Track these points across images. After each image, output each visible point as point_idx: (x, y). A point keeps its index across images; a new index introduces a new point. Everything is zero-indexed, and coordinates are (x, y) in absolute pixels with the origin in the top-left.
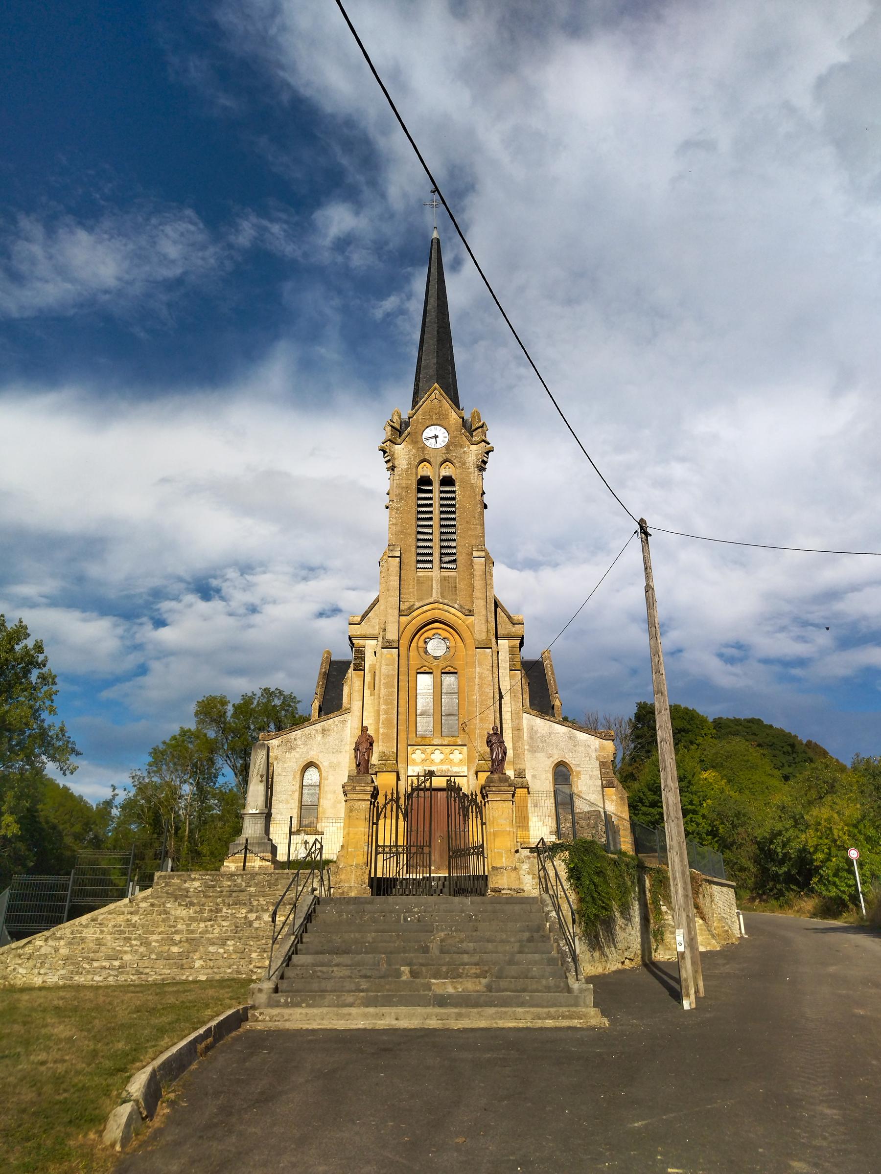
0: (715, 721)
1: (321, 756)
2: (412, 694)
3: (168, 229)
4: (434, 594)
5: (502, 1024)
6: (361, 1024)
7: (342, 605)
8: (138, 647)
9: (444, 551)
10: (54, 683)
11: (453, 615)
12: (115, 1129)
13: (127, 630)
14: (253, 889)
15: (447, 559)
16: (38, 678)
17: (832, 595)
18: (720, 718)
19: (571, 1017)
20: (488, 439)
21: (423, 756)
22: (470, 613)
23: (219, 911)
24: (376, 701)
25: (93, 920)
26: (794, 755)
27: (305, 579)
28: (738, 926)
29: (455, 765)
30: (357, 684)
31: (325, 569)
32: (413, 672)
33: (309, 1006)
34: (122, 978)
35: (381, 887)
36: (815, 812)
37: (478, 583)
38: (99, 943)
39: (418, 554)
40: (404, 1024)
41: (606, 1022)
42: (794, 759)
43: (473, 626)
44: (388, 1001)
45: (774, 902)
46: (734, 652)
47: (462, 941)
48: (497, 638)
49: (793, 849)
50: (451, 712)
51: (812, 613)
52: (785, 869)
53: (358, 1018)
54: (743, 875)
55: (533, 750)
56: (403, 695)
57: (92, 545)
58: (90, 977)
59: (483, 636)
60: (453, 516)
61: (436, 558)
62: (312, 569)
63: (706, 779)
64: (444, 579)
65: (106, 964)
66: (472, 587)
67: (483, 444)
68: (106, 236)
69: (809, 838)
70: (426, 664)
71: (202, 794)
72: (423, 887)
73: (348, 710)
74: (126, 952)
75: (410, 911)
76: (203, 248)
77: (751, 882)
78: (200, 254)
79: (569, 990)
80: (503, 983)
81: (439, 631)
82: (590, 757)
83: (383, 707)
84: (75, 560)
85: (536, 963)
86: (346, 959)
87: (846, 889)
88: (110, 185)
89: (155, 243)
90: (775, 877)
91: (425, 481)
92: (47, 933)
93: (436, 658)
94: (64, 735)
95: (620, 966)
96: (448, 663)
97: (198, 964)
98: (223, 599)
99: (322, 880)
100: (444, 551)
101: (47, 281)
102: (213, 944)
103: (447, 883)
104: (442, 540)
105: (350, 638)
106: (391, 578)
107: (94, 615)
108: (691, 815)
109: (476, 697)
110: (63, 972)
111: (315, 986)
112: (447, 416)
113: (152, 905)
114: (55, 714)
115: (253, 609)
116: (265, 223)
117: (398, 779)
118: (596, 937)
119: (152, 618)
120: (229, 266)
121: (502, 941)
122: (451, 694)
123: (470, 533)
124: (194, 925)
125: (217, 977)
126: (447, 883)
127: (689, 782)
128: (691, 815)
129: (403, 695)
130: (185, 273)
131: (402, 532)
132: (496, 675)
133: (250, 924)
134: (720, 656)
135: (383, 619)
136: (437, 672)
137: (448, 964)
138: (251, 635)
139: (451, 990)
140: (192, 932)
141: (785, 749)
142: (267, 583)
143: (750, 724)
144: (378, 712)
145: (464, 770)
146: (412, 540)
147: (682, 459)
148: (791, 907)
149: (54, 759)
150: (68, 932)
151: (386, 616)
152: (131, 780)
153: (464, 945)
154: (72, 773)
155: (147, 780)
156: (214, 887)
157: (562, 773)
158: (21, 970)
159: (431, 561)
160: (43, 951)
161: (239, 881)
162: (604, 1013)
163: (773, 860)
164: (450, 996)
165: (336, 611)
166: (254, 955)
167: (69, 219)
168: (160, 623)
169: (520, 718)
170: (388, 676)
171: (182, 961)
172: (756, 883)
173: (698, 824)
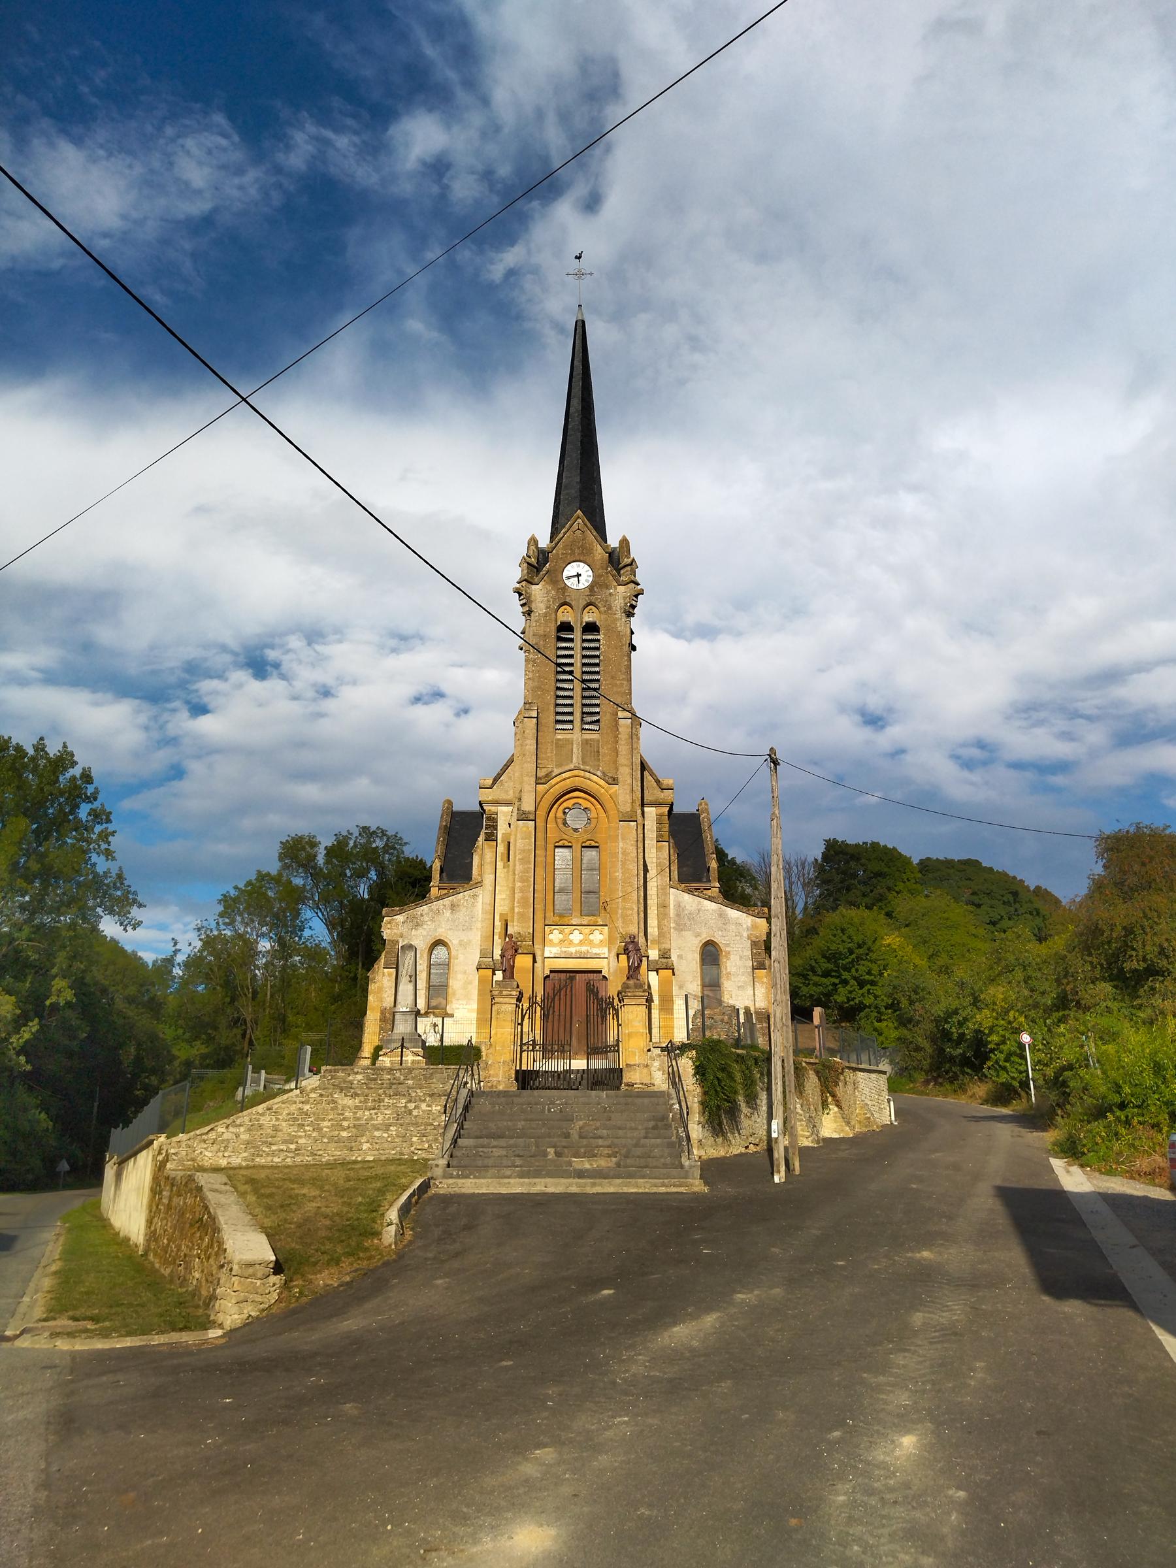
0: (922, 862)
1: (450, 933)
2: (550, 869)
3: (190, 143)
4: (575, 760)
5: (626, 1190)
6: (519, 1190)
7: (445, 688)
8: (172, 741)
9: (586, 710)
10: (109, 821)
11: (595, 782)
12: (389, 1234)
13: (155, 718)
14: (410, 1082)
15: (589, 719)
16: (89, 814)
17: (1112, 676)
18: (928, 859)
19: (680, 1186)
20: (638, 578)
21: (561, 936)
22: (614, 781)
23: (380, 1101)
24: (511, 878)
25: (268, 1109)
26: (1017, 906)
27: (394, 650)
28: (886, 1113)
29: (595, 946)
30: (489, 856)
31: (422, 638)
32: (550, 846)
33: (475, 1177)
34: (298, 1159)
35: (525, 1079)
36: (991, 990)
37: (623, 748)
38: (276, 1129)
39: (558, 713)
40: (551, 1190)
41: (706, 1189)
42: (1016, 910)
43: (617, 796)
44: (537, 1174)
45: (948, 1086)
46: (976, 753)
47: (597, 1129)
48: (643, 805)
49: (969, 1030)
50: (591, 889)
51: (1082, 701)
52: (960, 1051)
53: (516, 1186)
54: (919, 1056)
55: (680, 928)
56: (540, 872)
57: (99, 601)
58: (269, 1159)
59: (628, 808)
60: (597, 669)
61: (577, 717)
62: (403, 638)
63: (889, 945)
64: (586, 743)
65: (283, 1147)
66: (616, 752)
67: (632, 585)
68: (101, 153)
69: (983, 1019)
70: (565, 837)
71: (284, 949)
72: (563, 1080)
73: (479, 884)
74: (300, 1137)
75: (553, 1103)
76: (240, 171)
77: (926, 1064)
78: (236, 181)
79: (682, 1166)
80: (629, 1161)
81: (580, 801)
82: (742, 936)
83: (518, 884)
84: (72, 621)
85: (658, 1146)
86: (502, 1142)
87: (1016, 1075)
88: (103, 73)
89: (171, 164)
90: (952, 1059)
91: (566, 627)
92: (228, 1121)
93: (576, 830)
94: (122, 884)
95: (743, 1150)
96: (589, 837)
97: (365, 1146)
98: (283, 677)
99: (473, 1075)
100: (586, 710)
101: (20, 217)
102: (378, 1129)
103: (585, 1076)
104: (584, 697)
105: (480, 804)
106: (528, 742)
107: (109, 696)
108: (869, 986)
109: (619, 874)
110: (245, 1155)
111: (479, 1163)
112: (590, 551)
113: (321, 1095)
114: (114, 859)
115: (326, 692)
116: (328, 134)
117: (534, 961)
118: (720, 1124)
119: (188, 702)
120: (277, 199)
121: (631, 1128)
122: (592, 869)
123: (615, 689)
124: (360, 1113)
125: (383, 1158)
126: (585, 1076)
127: (869, 949)
128: (869, 986)
129: (540, 872)
130: (216, 210)
131: (539, 688)
132: (640, 850)
133: (410, 1112)
134: (956, 757)
135: (518, 787)
136: (577, 847)
137: (586, 1146)
138: (324, 728)
139: (587, 1166)
140: (358, 1119)
141: (1005, 899)
142: (343, 656)
143: (963, 867)
144: (513, 889)
145: (604, 951)
146: (550, 698)
147: (914, 488)
148: (964, 1091)
149: (111, 912)
150: (246, 1119)
151: (521, 783)
152: (196, 933)
153: (599, 1132)
154: (134, 929)
155: (216, 933)
156: (375, 1080)
157: (711, 954)
158: (207, 1153)
159: (571, 722)
160: (225, 1137)
161: (398, 1075)
162: (706, 1183)
163: (950, 1040)
164: (587, 1170)
165: (438, 695)
166: (414, 1139)
167: (46, 123)
168: (199, 709)
169: (667, 895)
170: (524, 851)
171: (351, 1145)
172: (931, 1065)
173: (876, 997)
